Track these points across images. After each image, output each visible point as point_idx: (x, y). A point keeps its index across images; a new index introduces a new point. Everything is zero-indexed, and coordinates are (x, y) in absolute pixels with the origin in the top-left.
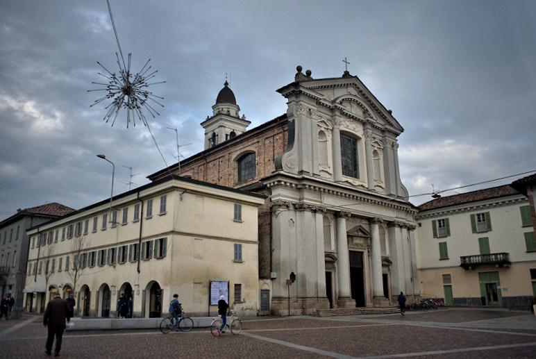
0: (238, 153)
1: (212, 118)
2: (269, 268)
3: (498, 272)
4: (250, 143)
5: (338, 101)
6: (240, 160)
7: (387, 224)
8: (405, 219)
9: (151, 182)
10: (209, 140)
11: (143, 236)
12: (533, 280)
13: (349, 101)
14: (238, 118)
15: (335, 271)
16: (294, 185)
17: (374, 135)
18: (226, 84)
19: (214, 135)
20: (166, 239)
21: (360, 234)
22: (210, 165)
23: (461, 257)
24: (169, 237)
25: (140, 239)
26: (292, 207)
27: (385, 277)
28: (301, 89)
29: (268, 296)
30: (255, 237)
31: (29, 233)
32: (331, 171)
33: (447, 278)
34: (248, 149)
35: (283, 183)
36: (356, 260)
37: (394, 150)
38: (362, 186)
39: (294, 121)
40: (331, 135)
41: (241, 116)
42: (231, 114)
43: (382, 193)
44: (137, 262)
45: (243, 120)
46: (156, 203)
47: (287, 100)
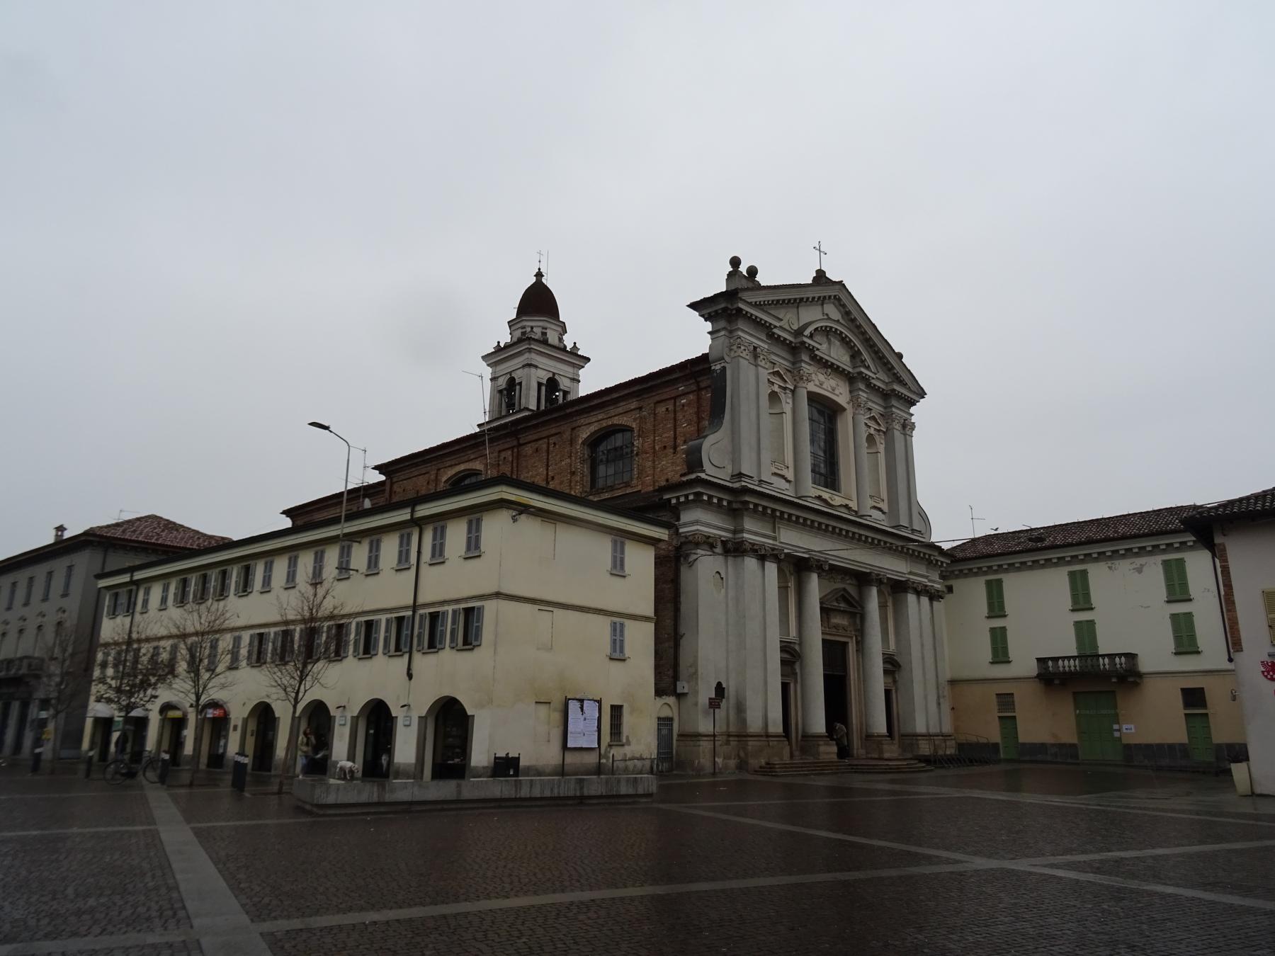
0: (593, 428)
1: (507, 346)
2: (671, 673)
3: (1113, 692)
4: (620, 410)
5: (807, 333)
6: (594, 442)
7: (891, 587)
8: (926, 577)
9: (383, 478)
10: (500, 392)
11: (421, 600)
12: (1188, 712)
13: (827, 332)
14: (564, 349)
15: (796, 682)
16: (725, 503)
17: (870, 404)
18: (539, 275)
19: (512, 383)
20: (480, 609)
21: (843, 605)
22: (528, 450)
23: (1039, 660)
24: (490, 607)
25: (415, 607)
26: (719, 550)
27: (888, 693)
28: (741, 305)
29: (671, 730)
30: (649, 610)
31: (103, 583)
32: (790, 475)
33: (1006, 701)
34: (616, 421)
35: (705, 498)
36: (835, 654)
37: (905, 435)
38: (846, 506)
39: (724, 368)
40: (790, 401)
41: (569, 347)
42: (550, 341)
43: (878, 520)
44: (406, 657)
45: (574, 352)
46: (456, 534)
47: (708, 326)
